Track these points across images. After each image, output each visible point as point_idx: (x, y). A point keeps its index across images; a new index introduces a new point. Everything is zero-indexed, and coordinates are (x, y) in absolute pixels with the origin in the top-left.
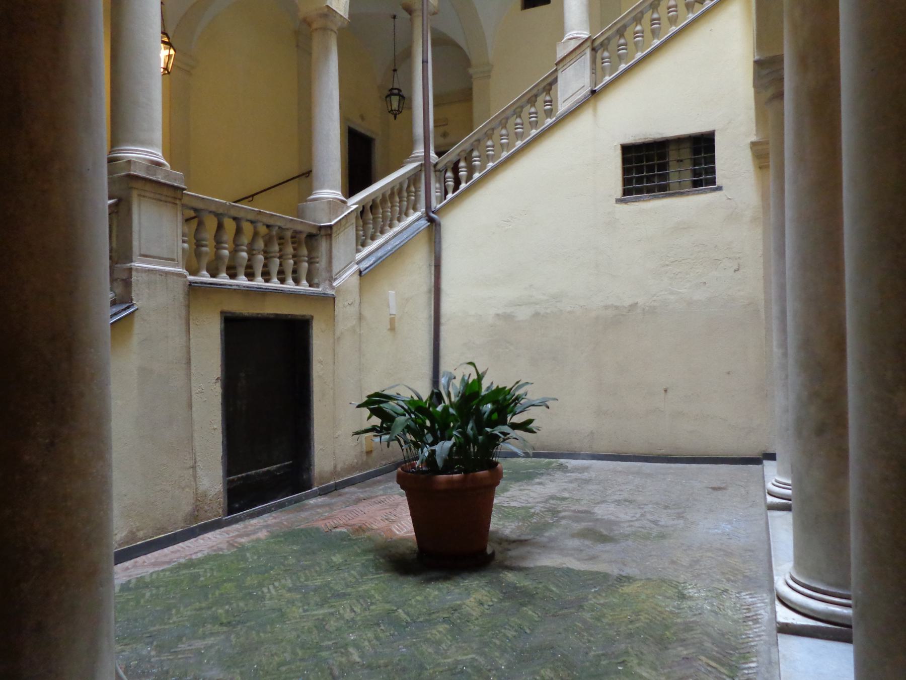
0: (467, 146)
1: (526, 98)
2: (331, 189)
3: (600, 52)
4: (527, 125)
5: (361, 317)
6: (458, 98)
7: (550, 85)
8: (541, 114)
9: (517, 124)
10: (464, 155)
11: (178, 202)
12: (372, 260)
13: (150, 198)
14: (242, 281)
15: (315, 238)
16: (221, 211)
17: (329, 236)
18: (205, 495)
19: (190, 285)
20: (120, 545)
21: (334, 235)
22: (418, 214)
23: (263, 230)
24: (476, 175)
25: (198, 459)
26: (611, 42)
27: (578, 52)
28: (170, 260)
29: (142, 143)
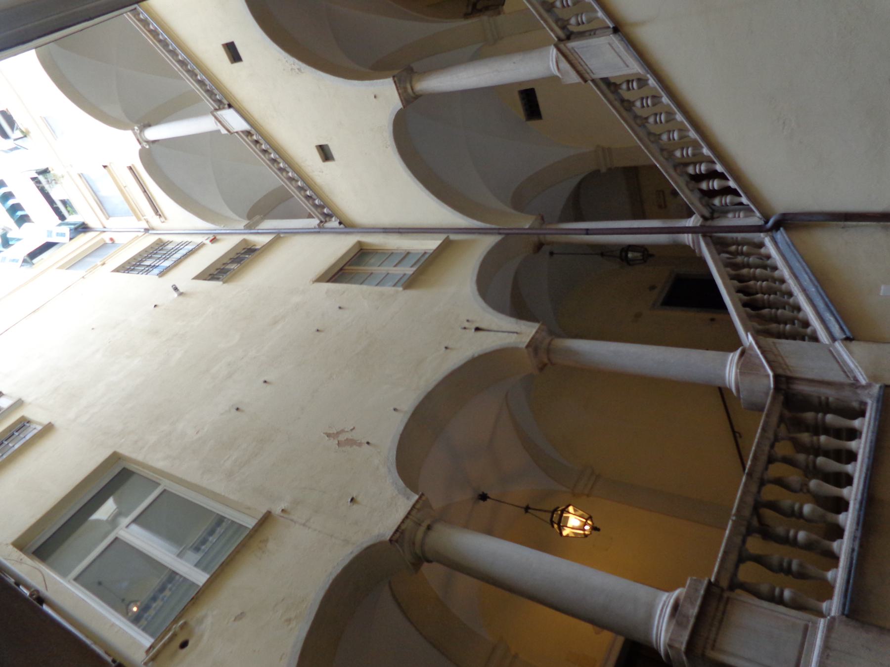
0: (682, 181)
1: (625, 113)
2: (725, 367)
3: (571, 28)
4: (657, 109)
6: (632, 187)
7: (610, 85)
8: (644, 92)
9: (656, 122)
10: (693, 184)
11: (726, 594)
12: (828, 316)
13: (717, 634)
14: (848, 520)
15: (793, 401)
16: (743, 529)
17: (790, 380)
19: (847, 616)
21: (789, 374)
22: (767, 241)
23: (777, 470)
24: (719, 168)
26: (560, 16)
27: (571, 57)
28: (806, 632)
29: (650, 617)
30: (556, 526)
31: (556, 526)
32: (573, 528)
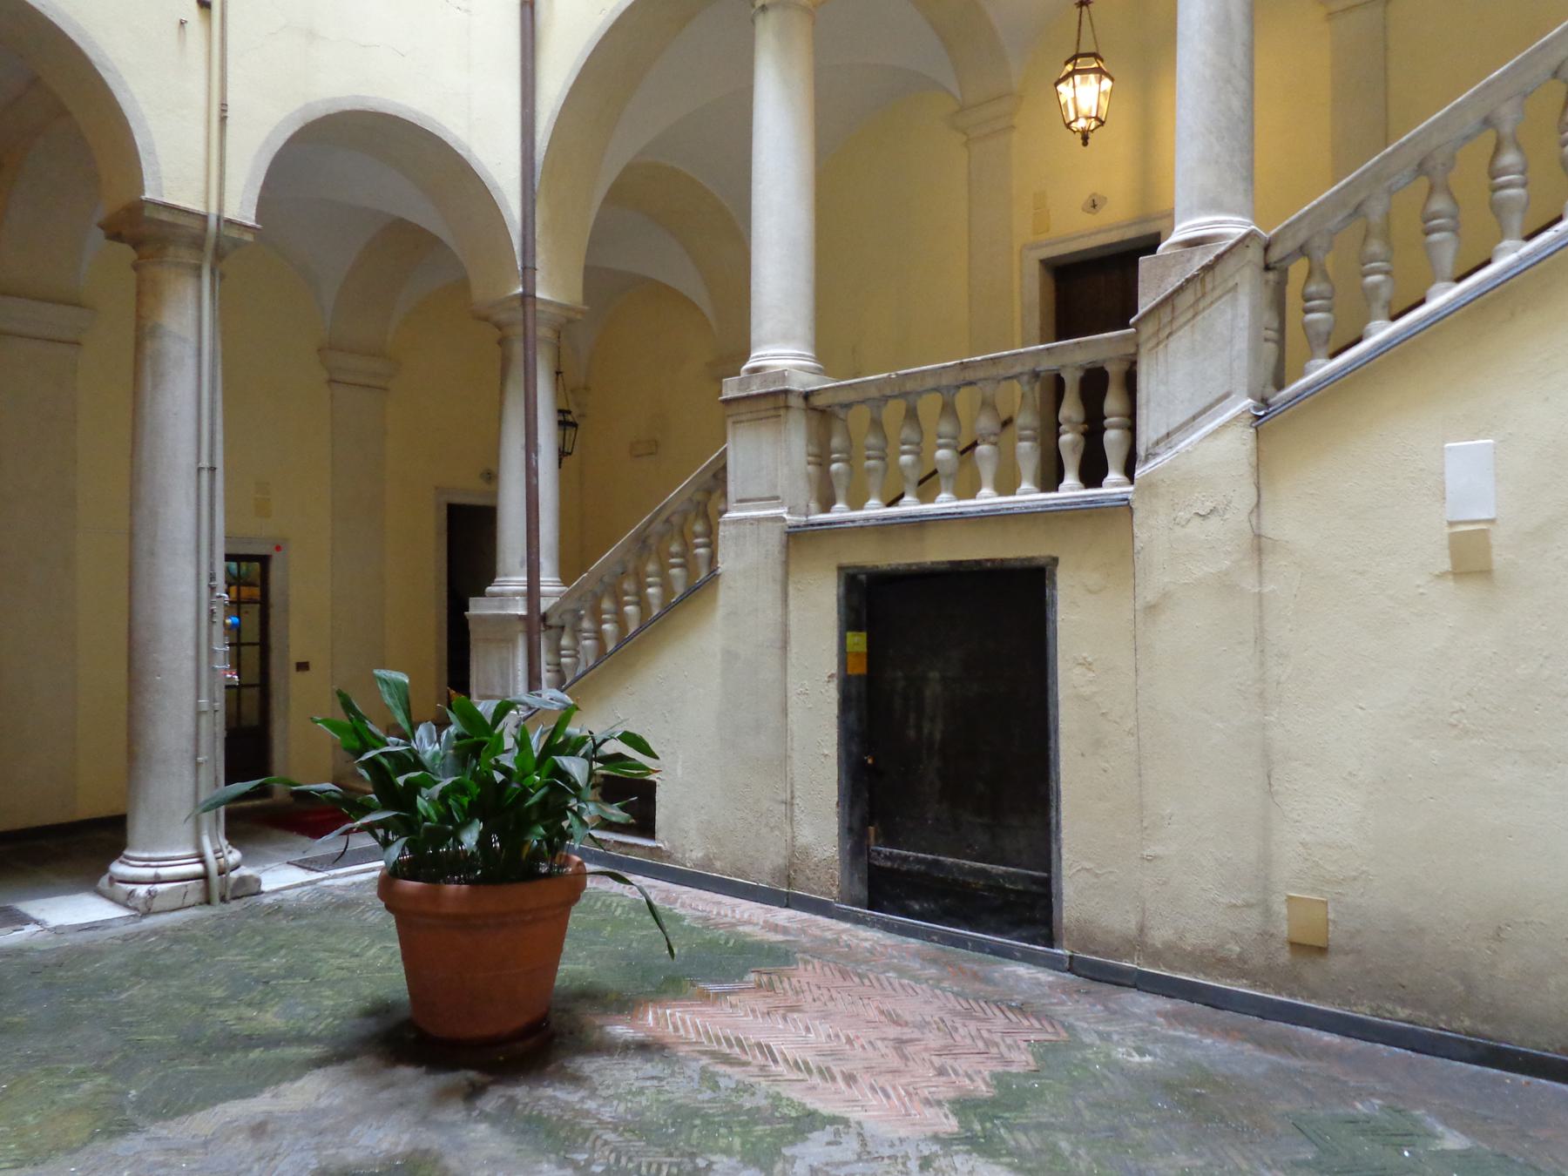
5: (1259, 546)
18: (806, 852)
20: (696, 866)
25: (797, 794)
30: (1069, 68)
31: (1069, 68)
32: (1075, 99)
